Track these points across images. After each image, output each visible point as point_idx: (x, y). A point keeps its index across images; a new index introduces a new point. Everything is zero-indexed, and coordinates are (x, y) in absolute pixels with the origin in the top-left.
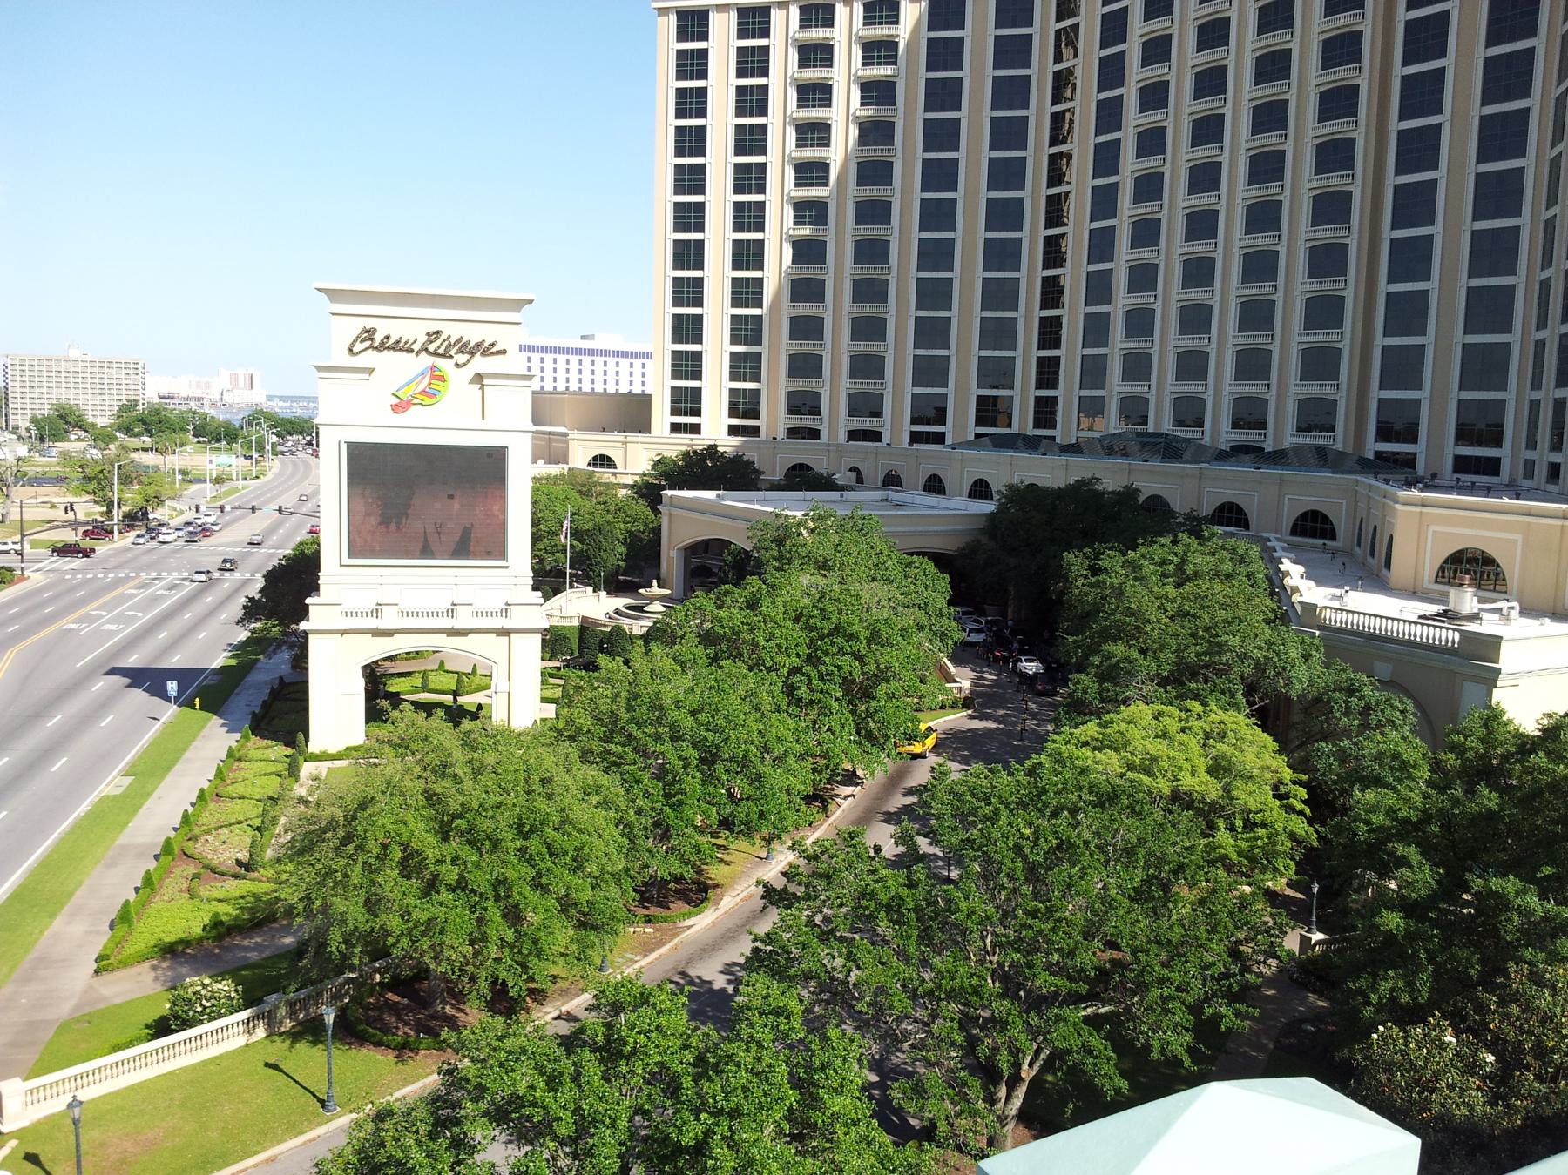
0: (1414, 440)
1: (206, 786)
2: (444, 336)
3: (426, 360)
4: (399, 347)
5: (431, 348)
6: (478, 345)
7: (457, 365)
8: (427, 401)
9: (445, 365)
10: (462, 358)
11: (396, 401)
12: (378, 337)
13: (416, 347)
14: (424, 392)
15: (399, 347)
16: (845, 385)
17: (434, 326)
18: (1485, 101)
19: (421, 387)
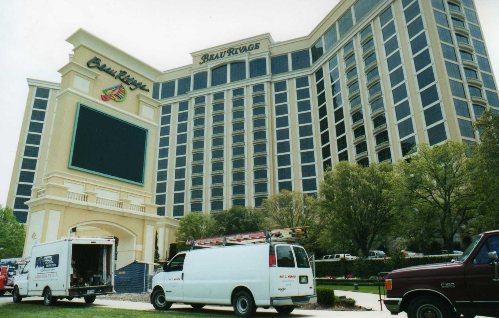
0: (280, 183)
1: (52, 76)
2: (127, 75)
3: (118, 82)
4: (109, 72)
5: (122, 78)
6: (139, 84)
7: (130, 88)
8: (117, 99)
9: (126, 87)
10: (133, 87)
11: (103, 94)
12: (102, 64)
13: (116, 74)
14: (116, 95)
15: (109, 72)
16: (297, 125)
17: (125, 70)
18: (161, 135)
19: (115, 93)
